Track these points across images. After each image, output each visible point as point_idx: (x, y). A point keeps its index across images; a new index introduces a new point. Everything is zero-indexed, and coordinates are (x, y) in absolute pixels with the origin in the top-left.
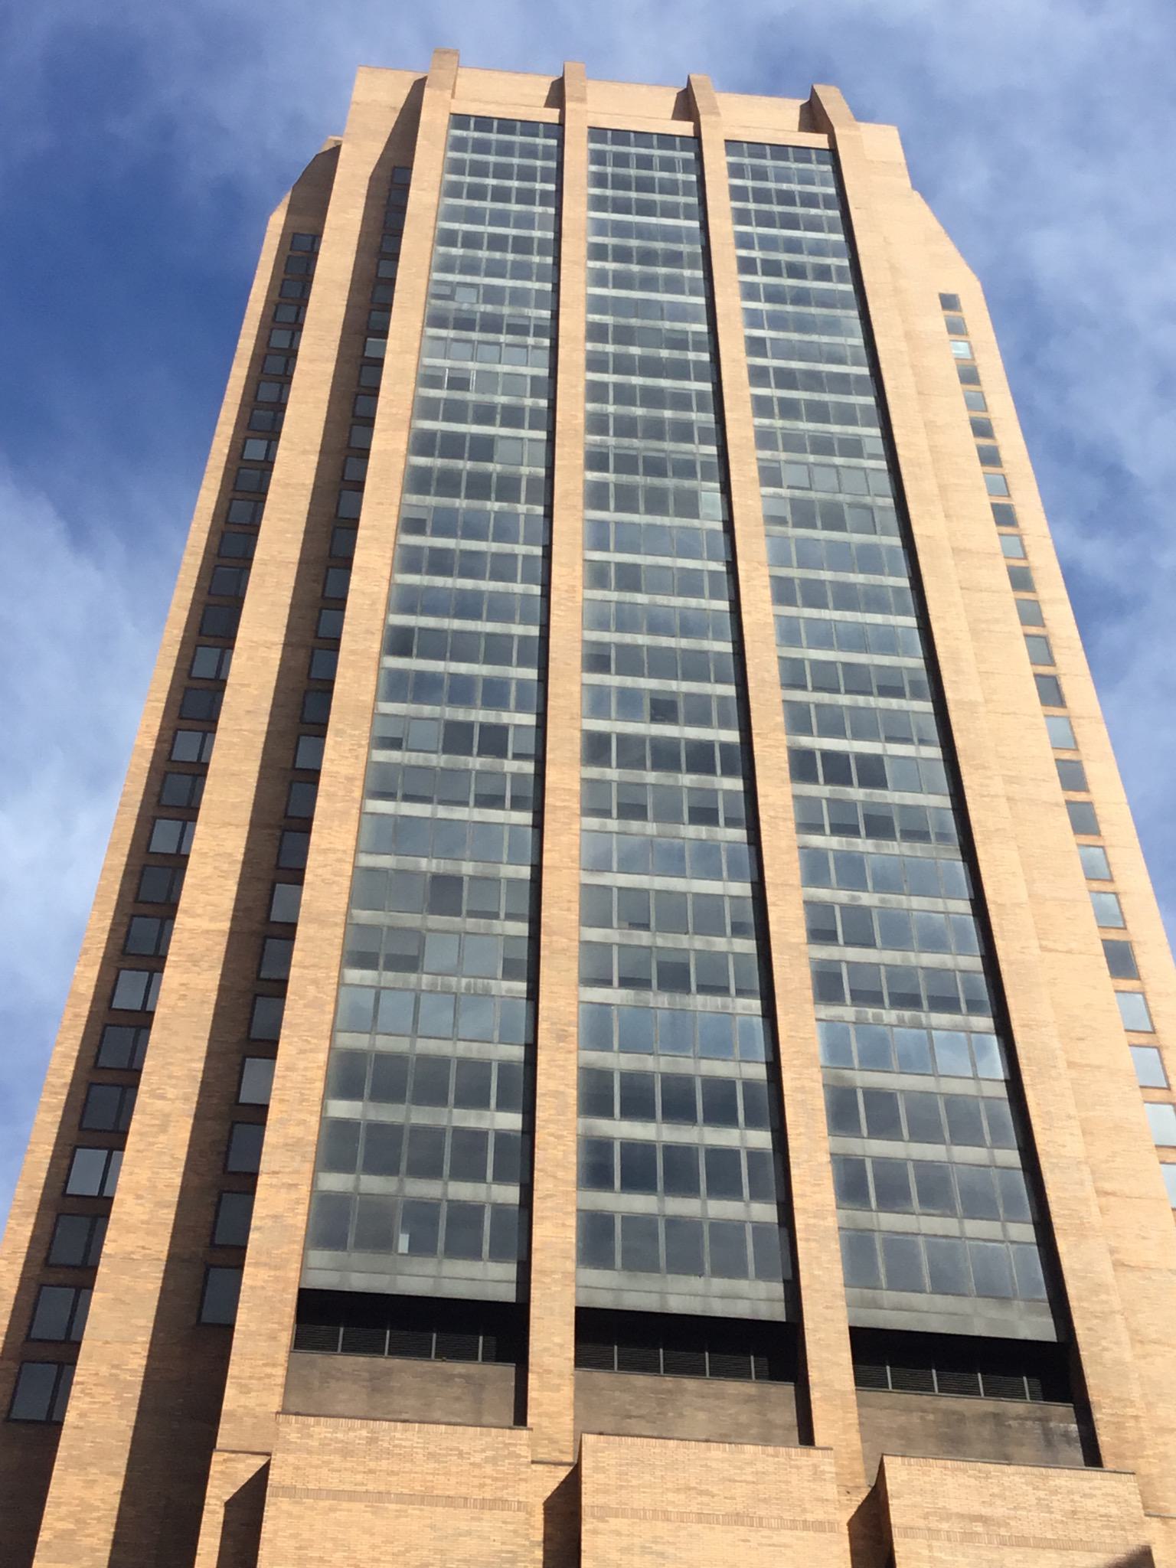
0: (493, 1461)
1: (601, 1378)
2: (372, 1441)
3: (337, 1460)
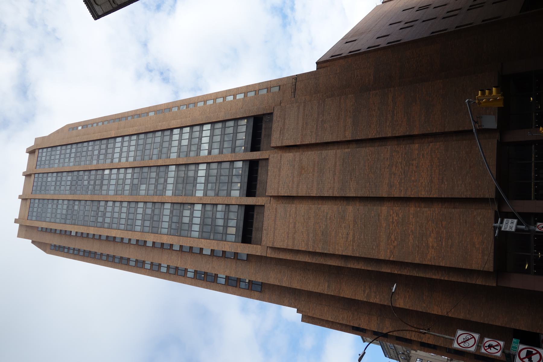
1: (257, 193)
2: (266, 230)
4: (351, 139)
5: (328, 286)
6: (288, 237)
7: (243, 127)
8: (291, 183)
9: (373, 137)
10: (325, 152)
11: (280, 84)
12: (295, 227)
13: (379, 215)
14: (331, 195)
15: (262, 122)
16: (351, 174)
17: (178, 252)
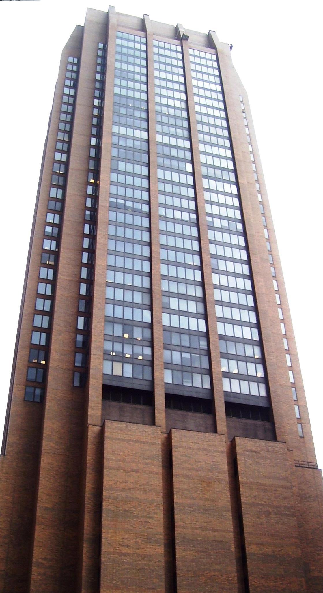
0: (153, 433)
1: (170, 411)
2: (127, 427)
3: (119, 431)
4: (247, 551)
5: (47, 509)
6: (120, 460)
7: (257, 390)
8: (190, 466)
9: (250, 582)
10: (229, 515)
11: (306, 437)
12: (132, 471)
13: (154, 589)
14: (176, 524)
15: (262, 420)
16: (203, 552)
17: (78, 276)
